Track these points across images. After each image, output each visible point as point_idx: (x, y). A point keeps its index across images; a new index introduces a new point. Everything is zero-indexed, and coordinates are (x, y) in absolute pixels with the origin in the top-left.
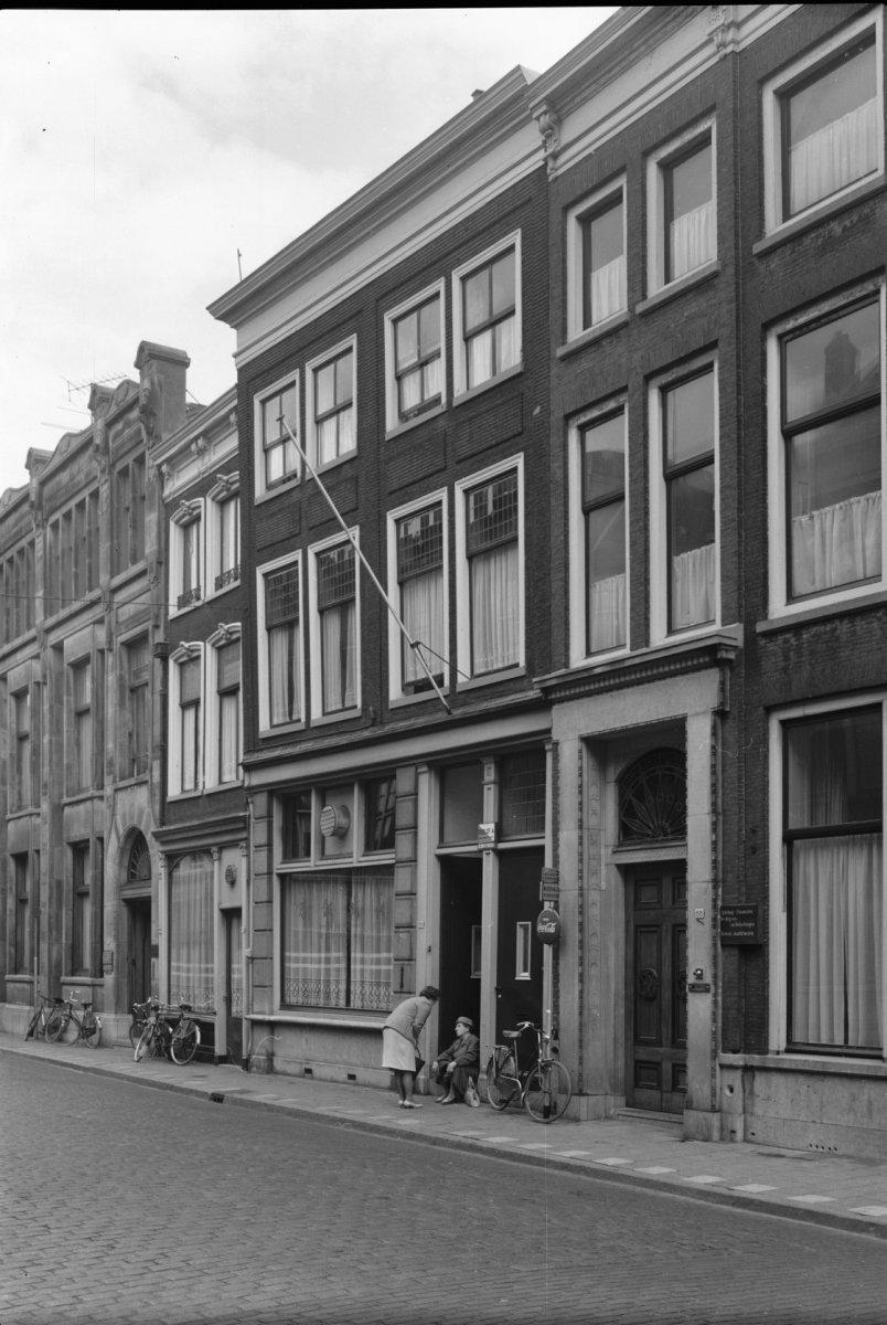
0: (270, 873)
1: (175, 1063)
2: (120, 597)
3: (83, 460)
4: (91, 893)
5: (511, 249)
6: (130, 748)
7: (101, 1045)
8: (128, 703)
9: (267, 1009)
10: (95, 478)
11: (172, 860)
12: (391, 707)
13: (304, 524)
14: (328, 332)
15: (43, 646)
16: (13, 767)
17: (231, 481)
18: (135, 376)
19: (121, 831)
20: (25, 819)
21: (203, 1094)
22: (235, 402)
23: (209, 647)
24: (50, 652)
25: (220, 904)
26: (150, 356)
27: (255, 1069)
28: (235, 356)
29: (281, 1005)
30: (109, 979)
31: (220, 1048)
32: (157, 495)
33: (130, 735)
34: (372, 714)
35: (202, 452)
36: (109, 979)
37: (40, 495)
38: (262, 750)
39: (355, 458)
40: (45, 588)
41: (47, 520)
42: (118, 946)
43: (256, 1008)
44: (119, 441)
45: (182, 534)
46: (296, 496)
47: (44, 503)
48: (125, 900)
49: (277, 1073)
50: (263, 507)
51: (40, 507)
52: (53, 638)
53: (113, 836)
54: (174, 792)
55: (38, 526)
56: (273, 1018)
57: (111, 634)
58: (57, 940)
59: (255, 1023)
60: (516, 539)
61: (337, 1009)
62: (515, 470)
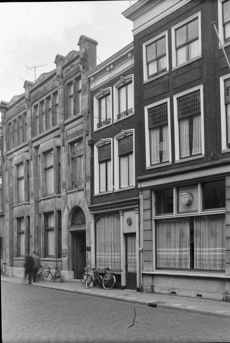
0: (151, 219)
1: (104, 289)
2: (67, 127)
3: (50, 82)
4: (25, 233)
5: (197, 18)
6: (72, 179)
7: (62, 281)
8: (71, 164)
9: (151, 269)
10: (57, 87)
11: (97, 218)
12: (222, 152)
13: (171, 87)
14: (184, 14)
15: (31, 147)
16: (16, 188)
17: (105, 91)
18: (77, 49)
19: (70, 208)
20: (22, 206)
21: (144, 304)
22: (133, 48)
23: (115, 139)
24: (33, 149)
25: (123, 231)
26: (84, 41)
27: (145, 291)
28: (133, 31)
29: (156, 268)
30: (65, 259)
31: (123, 283)
32: (88, 88)
33: (72, 174)
34: (212, 156)
35: (110, 71)
36: (65, 259)
37: (30, 97)
38: (147, 174)
39: (201, 59)
40: (32, 127)
41: (32, 104)
42: (68, 248)
43: (144, 269)
44: (68, 73)
45: (98, 102)
46: (165, 78)
47: (31, 99)
48: (71, 232)
49: (155, 293)
50: (148, 84)
51: (30, 100)
52: (35, 144)
53: (66, 210)
54: (96, 193)
55: (28, 107)
56: (152, 273)
57: (64, 140)
58: (37, 246)
59: (144, 275)
60: (200, 113)
61: (186, 270)
62: (199, 90)
